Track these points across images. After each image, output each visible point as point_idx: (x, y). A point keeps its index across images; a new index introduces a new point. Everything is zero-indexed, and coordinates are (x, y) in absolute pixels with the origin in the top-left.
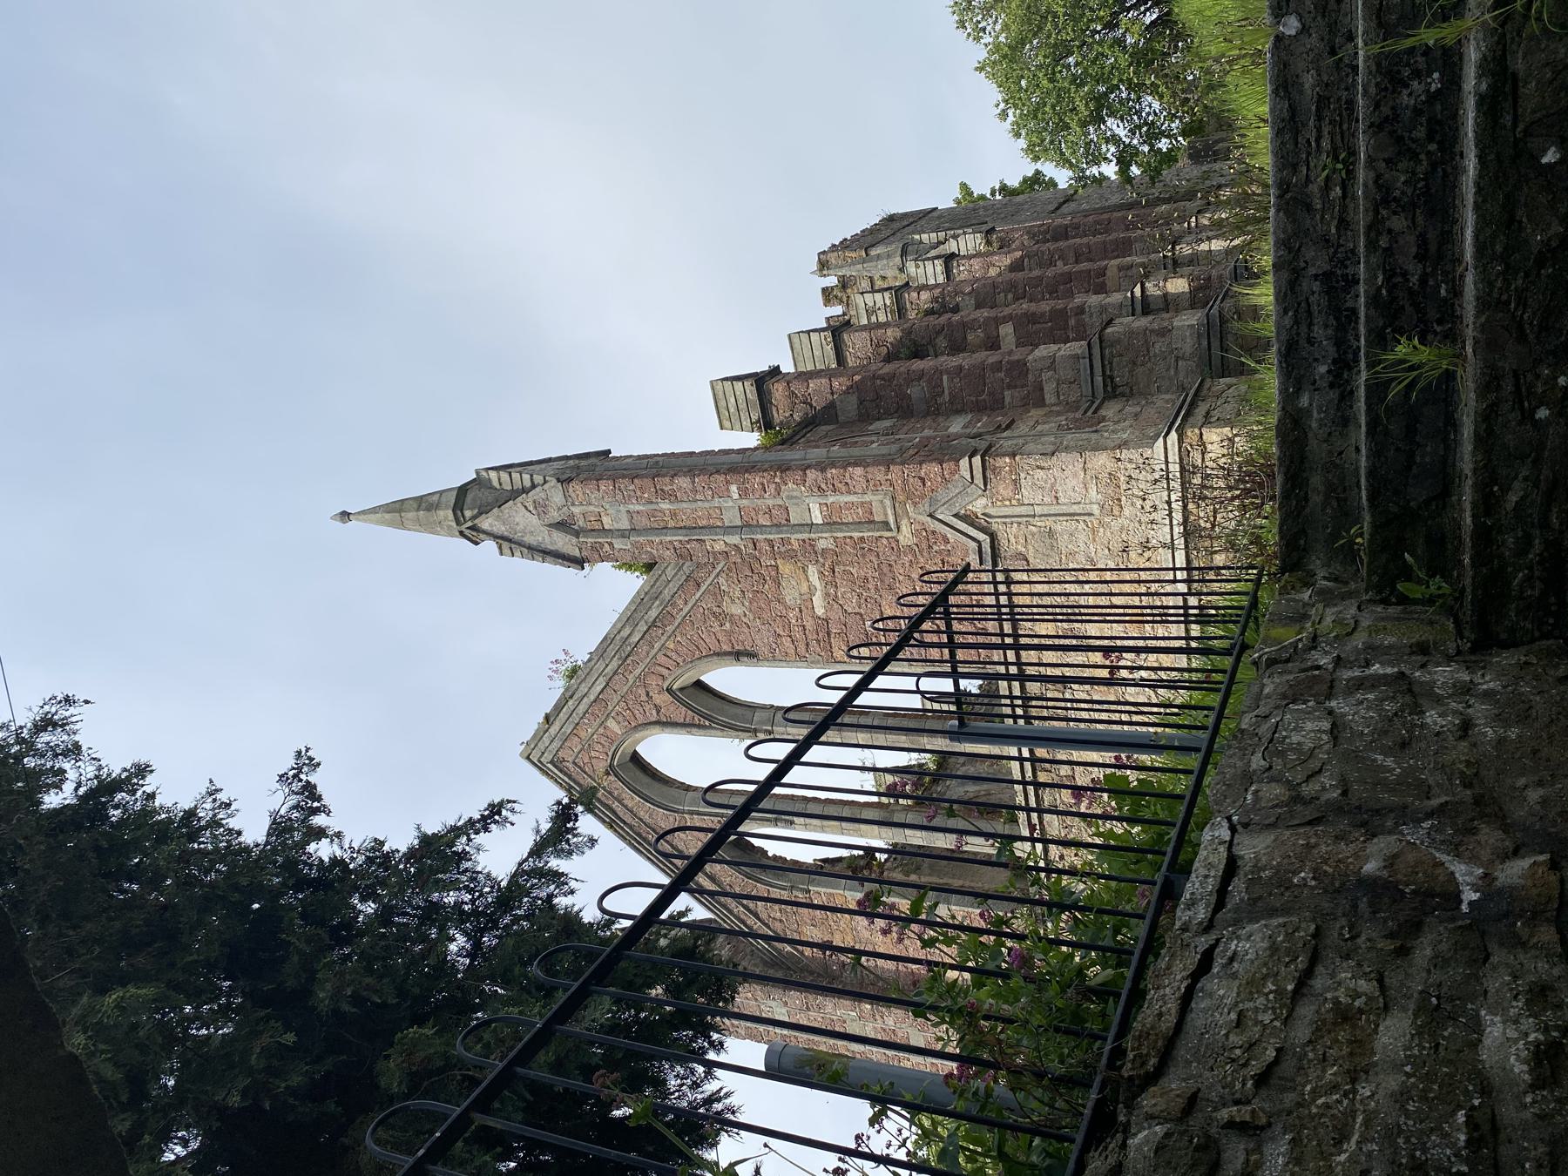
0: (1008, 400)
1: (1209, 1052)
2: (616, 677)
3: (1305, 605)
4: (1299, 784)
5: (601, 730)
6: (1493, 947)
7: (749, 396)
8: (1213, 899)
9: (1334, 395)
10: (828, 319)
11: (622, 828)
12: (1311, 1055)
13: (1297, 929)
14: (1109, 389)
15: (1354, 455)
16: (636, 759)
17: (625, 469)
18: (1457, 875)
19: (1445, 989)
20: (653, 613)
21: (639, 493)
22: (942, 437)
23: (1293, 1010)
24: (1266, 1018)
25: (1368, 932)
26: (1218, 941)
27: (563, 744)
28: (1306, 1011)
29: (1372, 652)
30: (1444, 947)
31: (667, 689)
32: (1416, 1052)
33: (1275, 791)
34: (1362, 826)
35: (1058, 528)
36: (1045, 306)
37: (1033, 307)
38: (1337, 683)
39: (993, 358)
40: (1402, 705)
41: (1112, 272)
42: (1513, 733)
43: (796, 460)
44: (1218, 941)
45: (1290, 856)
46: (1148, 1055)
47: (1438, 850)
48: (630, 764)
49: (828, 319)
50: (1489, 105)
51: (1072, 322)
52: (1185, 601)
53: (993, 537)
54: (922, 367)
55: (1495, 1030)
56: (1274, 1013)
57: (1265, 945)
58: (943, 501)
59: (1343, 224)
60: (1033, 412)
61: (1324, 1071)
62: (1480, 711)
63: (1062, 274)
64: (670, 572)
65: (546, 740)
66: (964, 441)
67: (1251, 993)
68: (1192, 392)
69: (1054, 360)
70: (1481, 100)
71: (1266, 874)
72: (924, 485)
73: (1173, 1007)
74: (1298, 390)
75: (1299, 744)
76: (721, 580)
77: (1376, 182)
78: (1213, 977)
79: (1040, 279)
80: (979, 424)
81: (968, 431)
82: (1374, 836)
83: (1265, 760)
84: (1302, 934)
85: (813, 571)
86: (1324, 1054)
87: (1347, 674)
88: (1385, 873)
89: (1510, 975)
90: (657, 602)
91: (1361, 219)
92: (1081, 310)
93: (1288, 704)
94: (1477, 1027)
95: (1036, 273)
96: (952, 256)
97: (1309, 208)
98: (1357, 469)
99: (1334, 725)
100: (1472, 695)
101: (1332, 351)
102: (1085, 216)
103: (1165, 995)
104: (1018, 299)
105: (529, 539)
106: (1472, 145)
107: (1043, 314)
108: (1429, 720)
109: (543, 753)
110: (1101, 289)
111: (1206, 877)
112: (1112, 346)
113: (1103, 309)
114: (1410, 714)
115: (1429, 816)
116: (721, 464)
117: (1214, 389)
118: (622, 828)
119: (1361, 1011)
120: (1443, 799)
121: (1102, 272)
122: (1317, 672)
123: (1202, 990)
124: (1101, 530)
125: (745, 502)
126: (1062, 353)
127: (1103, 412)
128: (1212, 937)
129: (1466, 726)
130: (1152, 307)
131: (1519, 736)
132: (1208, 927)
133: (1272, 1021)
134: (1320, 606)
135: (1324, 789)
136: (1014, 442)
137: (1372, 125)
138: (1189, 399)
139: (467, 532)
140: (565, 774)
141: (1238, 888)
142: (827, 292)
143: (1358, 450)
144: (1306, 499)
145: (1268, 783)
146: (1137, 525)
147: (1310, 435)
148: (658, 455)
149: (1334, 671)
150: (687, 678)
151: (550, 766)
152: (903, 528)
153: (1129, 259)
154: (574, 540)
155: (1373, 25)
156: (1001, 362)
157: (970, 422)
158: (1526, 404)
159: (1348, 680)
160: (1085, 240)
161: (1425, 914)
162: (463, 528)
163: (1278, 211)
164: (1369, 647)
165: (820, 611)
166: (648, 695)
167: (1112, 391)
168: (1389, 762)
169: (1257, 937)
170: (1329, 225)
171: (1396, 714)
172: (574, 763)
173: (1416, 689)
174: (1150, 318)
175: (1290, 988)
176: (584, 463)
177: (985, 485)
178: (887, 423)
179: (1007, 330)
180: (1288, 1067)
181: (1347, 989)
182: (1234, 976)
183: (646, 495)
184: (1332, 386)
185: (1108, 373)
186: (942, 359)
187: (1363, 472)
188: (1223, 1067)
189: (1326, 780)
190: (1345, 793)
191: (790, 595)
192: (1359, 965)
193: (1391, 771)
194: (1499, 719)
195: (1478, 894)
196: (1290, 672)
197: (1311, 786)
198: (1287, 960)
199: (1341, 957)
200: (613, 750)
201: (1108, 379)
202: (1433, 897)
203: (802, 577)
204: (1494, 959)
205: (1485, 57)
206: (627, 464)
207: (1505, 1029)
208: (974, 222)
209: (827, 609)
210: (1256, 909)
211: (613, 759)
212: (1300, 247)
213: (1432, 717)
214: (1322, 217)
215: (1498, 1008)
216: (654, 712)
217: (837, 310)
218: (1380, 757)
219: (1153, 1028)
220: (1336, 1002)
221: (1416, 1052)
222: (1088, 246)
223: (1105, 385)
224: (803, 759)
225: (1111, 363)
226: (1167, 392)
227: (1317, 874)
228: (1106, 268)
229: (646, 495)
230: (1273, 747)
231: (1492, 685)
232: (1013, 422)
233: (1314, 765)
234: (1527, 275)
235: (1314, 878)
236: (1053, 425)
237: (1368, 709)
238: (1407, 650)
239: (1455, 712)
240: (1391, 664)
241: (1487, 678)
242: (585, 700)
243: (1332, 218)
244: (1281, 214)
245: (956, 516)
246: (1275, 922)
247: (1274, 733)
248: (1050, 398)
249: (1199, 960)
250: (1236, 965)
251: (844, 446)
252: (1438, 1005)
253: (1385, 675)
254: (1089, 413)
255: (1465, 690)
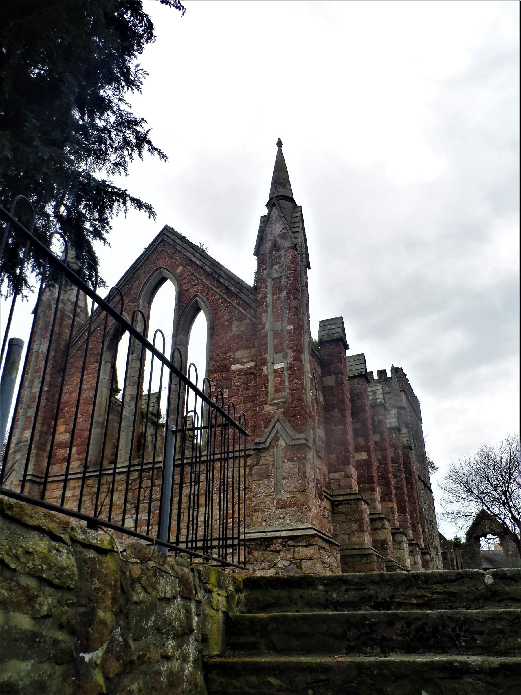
0: (331, 456)
1: (14, 539)
2: (202, 270)
3: (227, 588)
4: (140, 582)
5: (177, 263)
6: (64, 667)
7: (336, 335)
8: (86, 542)
9: (323, 601)
10: (371, 372)
11: (131, 273)
12: (13, 584)
13: (72, 579)
14: (336, 503)
15: (295, 609)
16: (163, 280)
17: (301, 276)
18: (97, 652)
19: (43, 645)
20: (233, 289)
21: (290, 282)
22: (315, 425)
23: (34, 577)
24: (30, 565)
25: (71, 611)
26: (67, 544)
27: (171, 245)
28: (32, 583)
29: (204, 618)
30: (63, 645)
31: (196, 295)
32: (14, 631)
33: (136, 571)
34: (120, 610)
35: (271, 479)
36: (375, 474)
37: (374, 468)
38: (188, 601)
39: (351, 448)
40: (178, 630)
41: (390, 505)
42: (164, 679)
43: (304, 356)
44: (67, 544)
45: (106, 577)
46: (13, 511)
47: (109, 643)
48: (161, 277)
49: (371, 372)
50: (448, 667)
51: (367, 486)
52: (236, 538)
53: (267, 449)
54: (347, 416)
55: (26, 666)
56: (32, 568)
57: (64, 565)
58: (284, 426)
59: (399, 605)
60: (326, 468)
61: (5, 590)
62: (176, 665)
63: (389, 481)
64: (251, 296)
65: (173, 237)
66: (312, 436)
67: (41, 558)
68: (334, 541)
69: (349, 477)
70: (451, 663)
71: (98, 567)
72: (292, 417)
73: (35, 522)
74: (326, 585)
75: (159, 583)
76: (248, 321)
77: (416, 618)
78: (49, 541)
79: (388, 471)
80: (320, 443)
81: (317, 437)
82: (115, 616)
83: (152, 567)
84: (69, 582)
85: (252, 364)
86: (13, 590)
87: (193, 606)
88: (97, 620)
89: (50, 674)
90: (238, 290)
91: (401, 611)
92: (373, 490)
93: (179, 578)
94: (25, 658)
95: (391, 469)
96: (400, 431)
97: (407, 589)
98: (288, 611)
99: (168, 599)
100: (182, 661)
101: (342, 600)
102: (417, 492)
103: (41, 519)
104: (379, 461)
105: (268, 230)
106: (431, 659)
107: (371, 472)
108: (170, 641)
109: (167, 236)
110: (383, 499)
111: (97, 539)
112: (356, 504)
113: (373, 500)
114: (174, 634)
115: (125, 641)
116: (303, 321)
117: (335, 551)
118: (131, 273)
119: (33, 607)
120: (133, 647)
121: (391, 500)
122: (194, 592)
123: (43, 536)
124: (270, 499)
125: (285, 332)
126: (353, 481)
127: (325, 500)
128: (69, 542)
129: (167, 658)
130: (374, 523)
131: (162, 682)
132: (74, 540)
133: (28, 567)
134: (225, 594)
135: (138, 594)
136: (311, 459)
137: (442, 616)
138: (330, 539)
139: (272, 201)
140: (157, 246)
141: (91, 554)
142: (384, 371)
143: (297, 611)
144: (275, 589)
145: (141, 568)
146: (272, 516)
147: (305, 591)
148: (307, 290)
149: (195, 600)
150: (201, 304)
151: (161, 239)
152: (272, 407)
153: (397, 512)
154: (267, 251)
155: (487, 616)
156: (349, 453)
157: (321, 438)
158: (314, 685)
159: (190, 606)
160: (406, 492)
161: (79, 637)
162: (274, 200)
163: (406, 575)
164: (205, 616)
165: (233, 367)
166: (194, 285)
167: (334, 505)
168: (151, 623)
169: (68, 562)
170: (400, 598)
171: (173, 627)
172: (163, 250)
173: (185, 637)
174: (368, 521)
175: (44, 576)
176: (304, 256)
177: (291, 445)
178: (322, 399)
179: (364, 456)
180: (8, 574)
181: (44, 601)
182: (50, 551)
183: (288, 286)
184: (327, 600)
185: (343, 502)
186: (351, 426)
187: (286, 614)
188: (7, 544)
189: (142, 595)
190: (136, 603)
191: (240, 354)
192: (55, 607)
193: (147, 623)
194: (171, 674)
195: (88, 661)
196: (194, 580)
197: (139, 588)
198: (57, 575)
199: (58, 599)
200: (168, 268)
201: (341, 502)
202: (87, 640)
203: (249, 359)
204: (57, 667)
205: (470, 664)
206: (303, 277)
207: (24, 671)
208: (415, 441)
209: (234, 372)
210: (81, 562)
211: (164, 268)
212: (390, 585)
213: (171, 643)
214: (403, 595)
215: (34, 668)
216: (185, 288)
217: (376, 377)
218: (153, 619)
219: (26, 514)
220: (37, 596)
221: (14, 631)
222: (403, 493)
223: (337, 501)
224: (155, 357)
225: (348, 504)
226: (334, 530)
227: (98, 589)
228: (392, 502)
229: (288, 286)
230: (157, 572)
231: (187, 671)
232: (321, 458)
233: (150, 590)
234: (373, 685)
235: (96, 588)
236: (319, 477)
237: (176, 615)
238: (204, 633)
239: (174, 653)
240: (198, 626)
241: (190, 669)
242: (192, 256)
243: (402, 599)
244: (405, 576)
245: (277, 432)
246: (75, 569)
247: (165, 572)
248: (332, 476)
249: (57, 535)
250: (55, 552)
251: (311, 379)
252: (36, 642)
253: (192, 623)
254: (325, 494)
255: (185, 658)
